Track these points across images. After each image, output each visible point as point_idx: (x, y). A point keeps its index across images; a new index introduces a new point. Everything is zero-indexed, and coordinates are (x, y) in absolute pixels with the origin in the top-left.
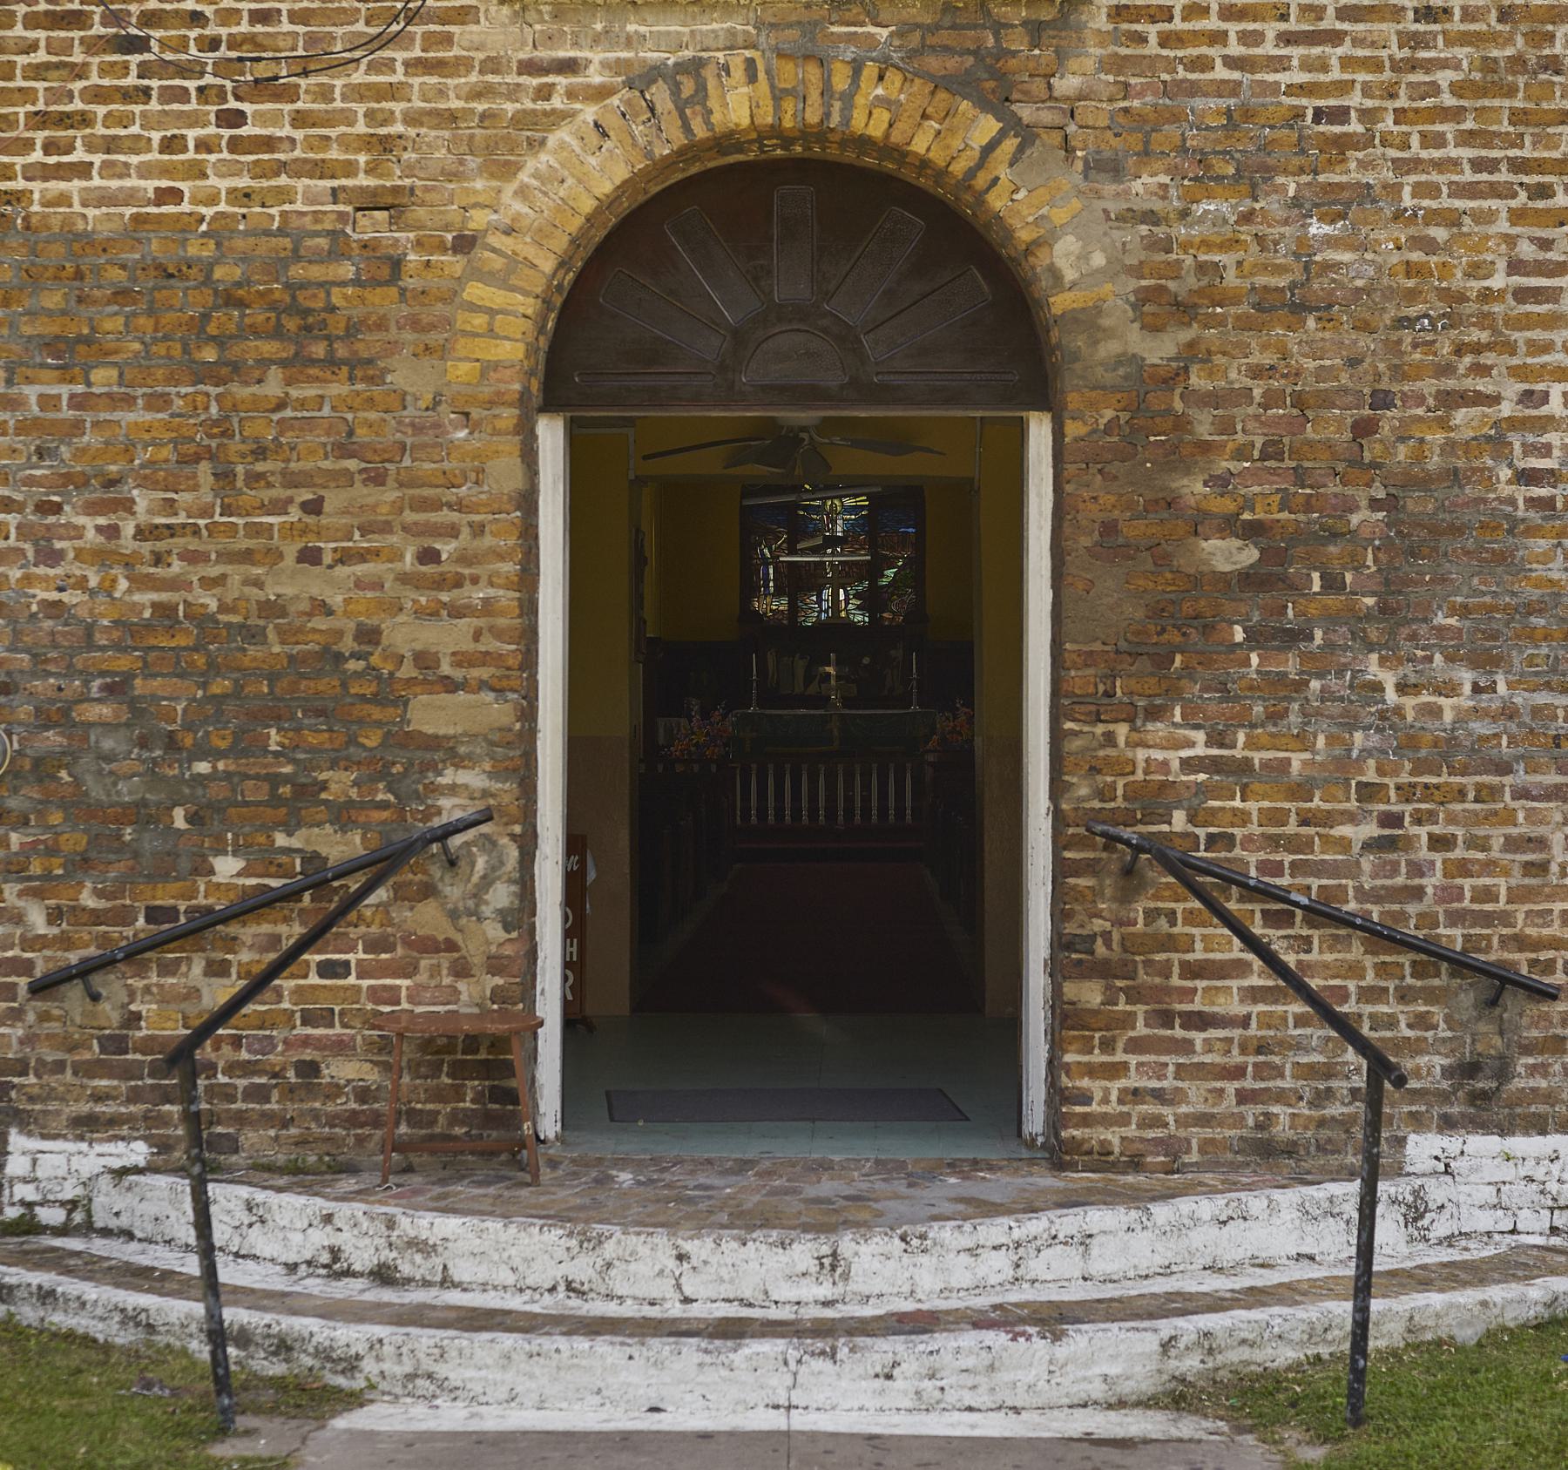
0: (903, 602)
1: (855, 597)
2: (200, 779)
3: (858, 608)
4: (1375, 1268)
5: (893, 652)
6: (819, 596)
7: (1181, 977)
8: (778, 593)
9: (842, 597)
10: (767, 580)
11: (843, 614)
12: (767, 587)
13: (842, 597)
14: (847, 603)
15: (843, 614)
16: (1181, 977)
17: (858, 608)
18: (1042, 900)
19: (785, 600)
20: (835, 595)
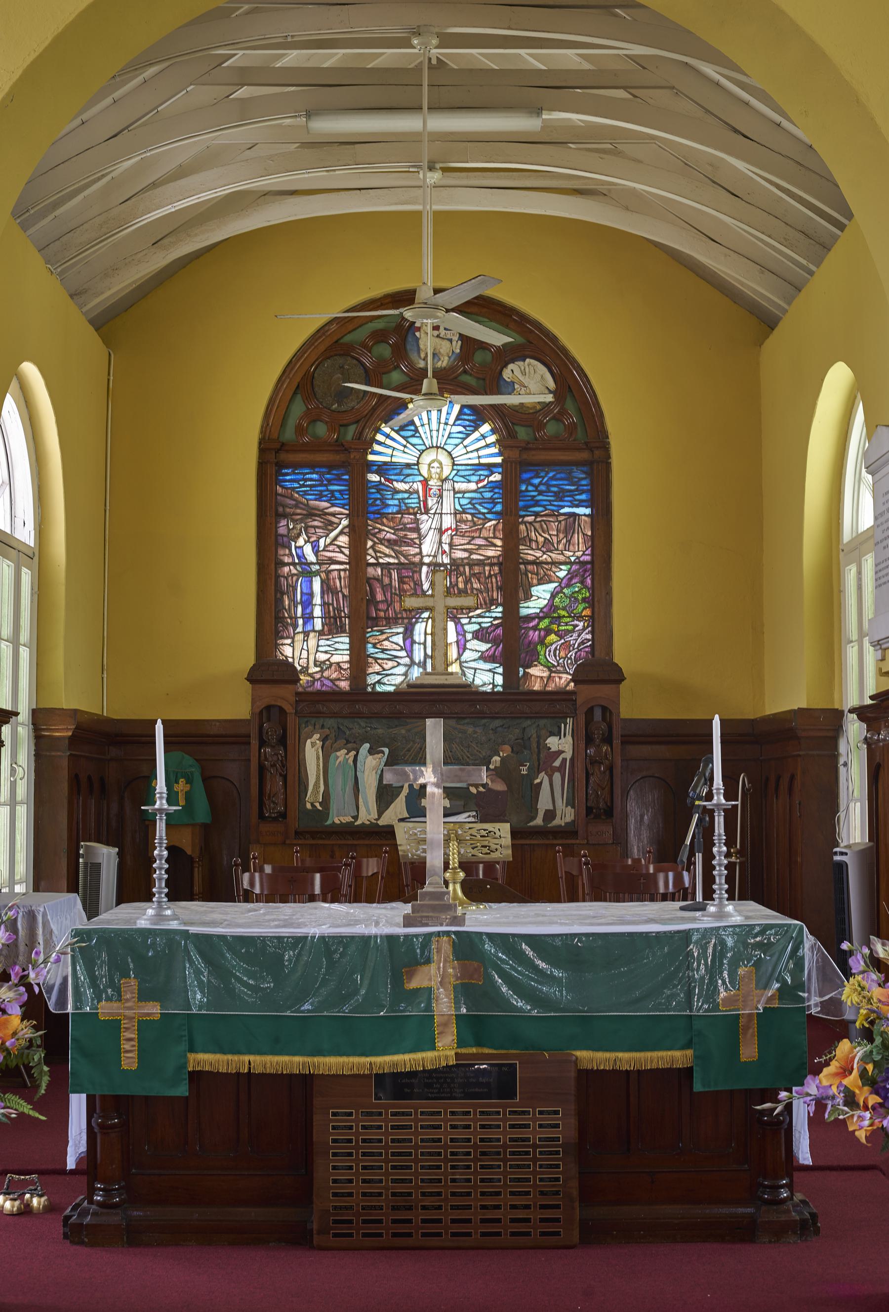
0: (567, 646)
1: (477, 635)
2: (189, 973)
3: (484, 657)
4: (10, 709)
5: (553, 743)
6: (408, 633)
7: (382, 1152)
8: (332, 627)
9: (452, 636)
10: (308, 603)
11: (454, 668)
12: (308, 618)
13: (452, 636)
14: (462, 647)
15: (454, 668)
16: (382, 1152)
17: (484, 657)
18: (524, 308)
19: (343, 642)
20: (438, 635)
